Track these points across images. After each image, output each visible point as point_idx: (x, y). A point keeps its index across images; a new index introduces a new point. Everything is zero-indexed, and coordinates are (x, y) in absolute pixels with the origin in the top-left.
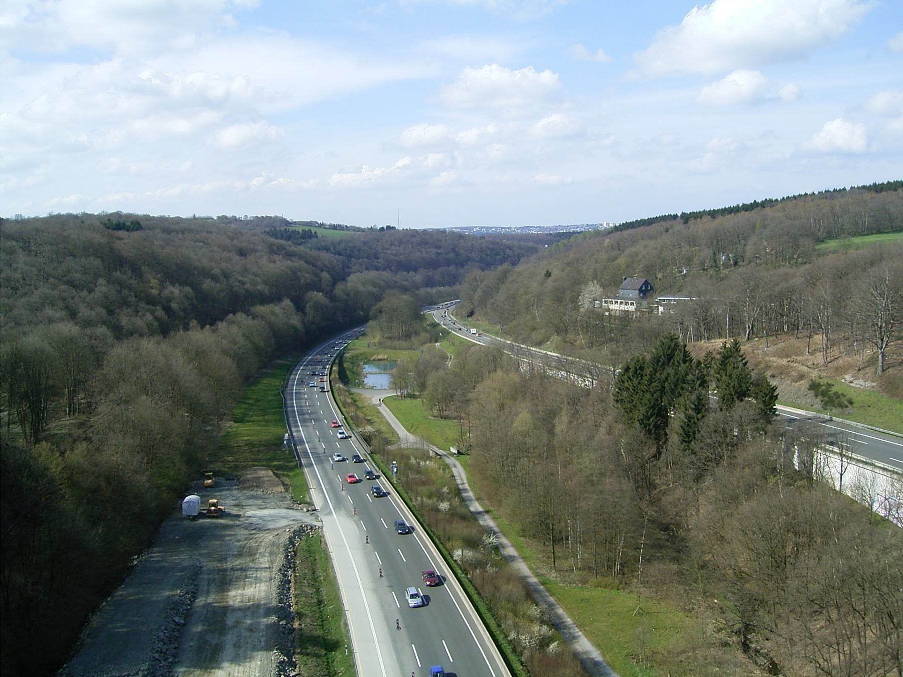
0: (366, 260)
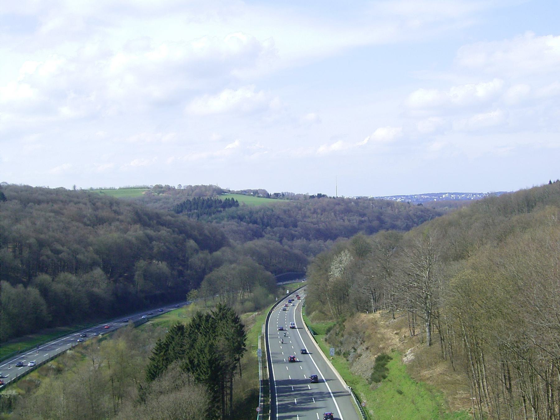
0: (282, 228)
